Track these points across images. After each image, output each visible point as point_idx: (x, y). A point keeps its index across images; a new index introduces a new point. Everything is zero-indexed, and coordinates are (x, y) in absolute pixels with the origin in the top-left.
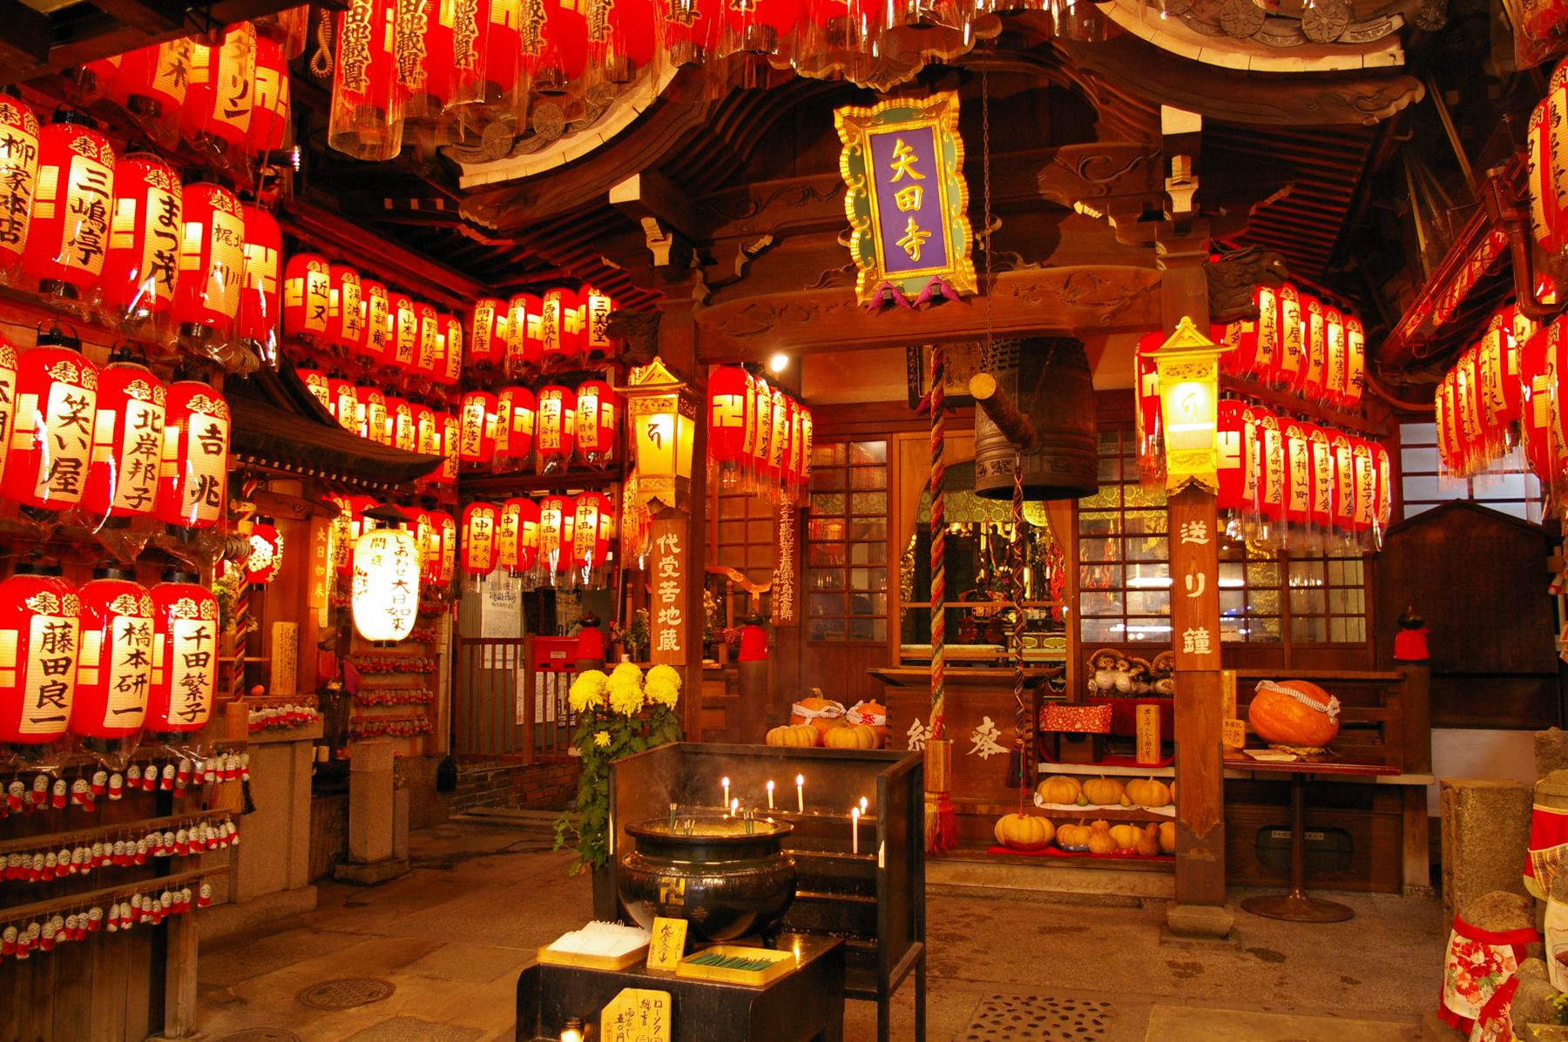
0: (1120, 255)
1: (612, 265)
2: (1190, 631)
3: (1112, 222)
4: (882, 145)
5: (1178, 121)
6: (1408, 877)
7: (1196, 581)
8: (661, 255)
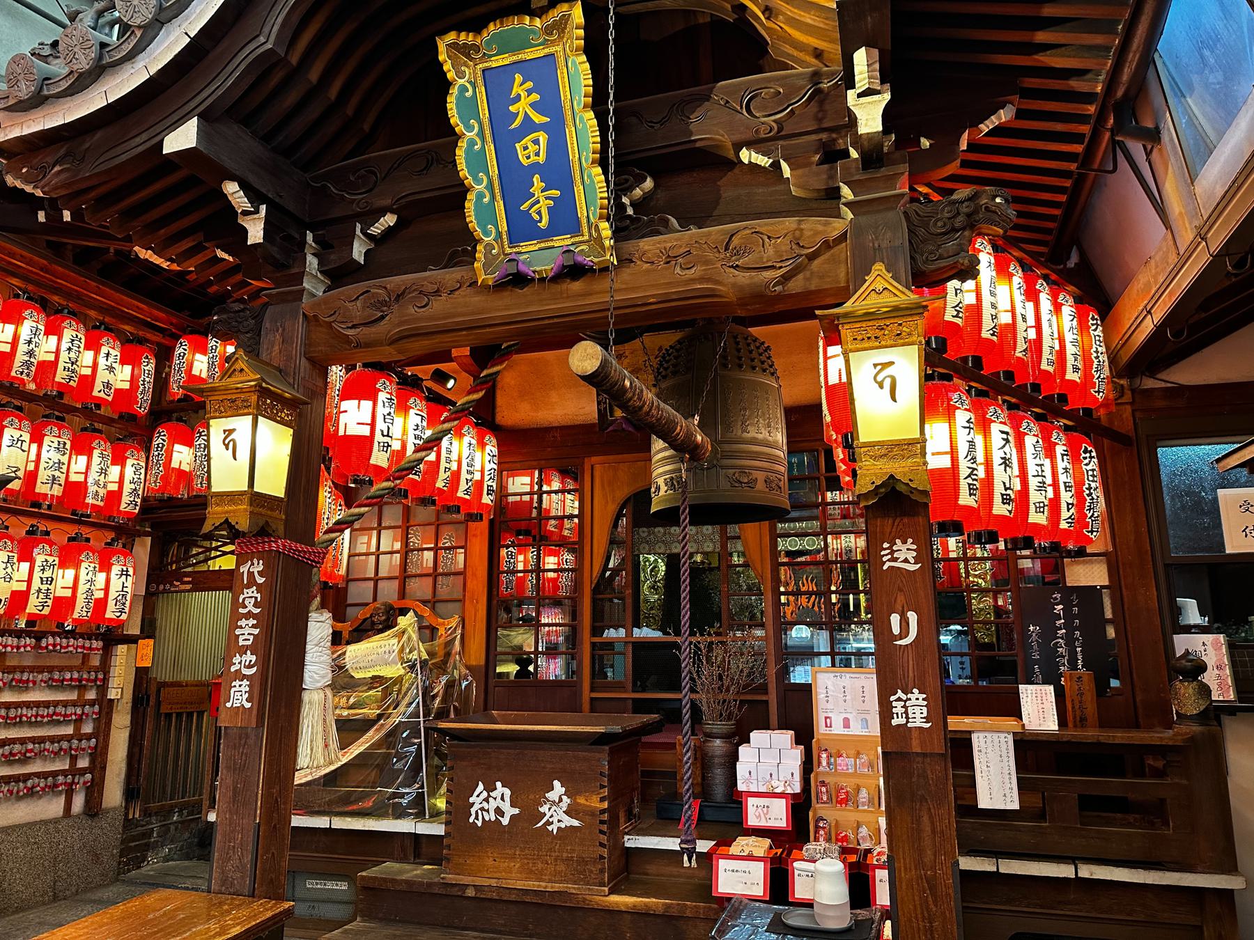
0: (801, 208)
1: (226, 256)
2: (900, 694)
4: (497, 83)
7: (905, 623)
8: (255, 232)
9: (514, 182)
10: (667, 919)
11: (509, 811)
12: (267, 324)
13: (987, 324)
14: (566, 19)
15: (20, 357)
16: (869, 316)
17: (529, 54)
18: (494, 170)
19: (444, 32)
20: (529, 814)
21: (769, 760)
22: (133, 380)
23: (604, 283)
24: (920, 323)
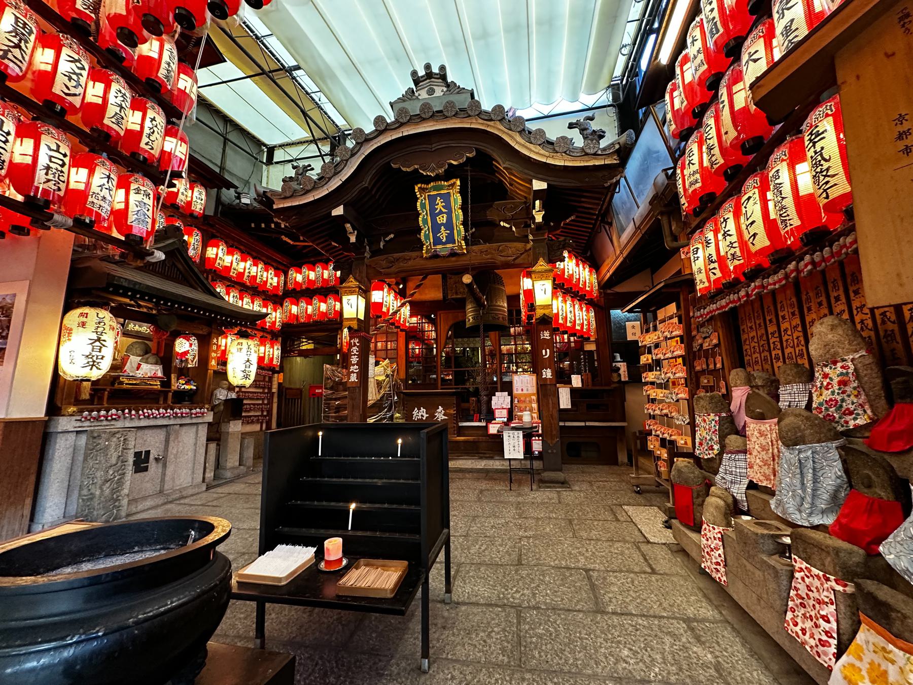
0: (517, 240)
3: (514, 229)
4: (432, 199)
5: (539, 185)
6: (620, 460)
8: (353, 239)
9: (436, 228)
10: (474, 442)
11: (426, 416)
12: (354, 267)
13: (566, 274)
14: (455, 183)
15: (246, 274)
16: (539, 272)
17: (442, 192)
18: (430, 225)
19: (417, 184)
20: (432, 416)
21: (501, 400)
22: (278, 283)
23: (464, 258)
24: (552, 274)
